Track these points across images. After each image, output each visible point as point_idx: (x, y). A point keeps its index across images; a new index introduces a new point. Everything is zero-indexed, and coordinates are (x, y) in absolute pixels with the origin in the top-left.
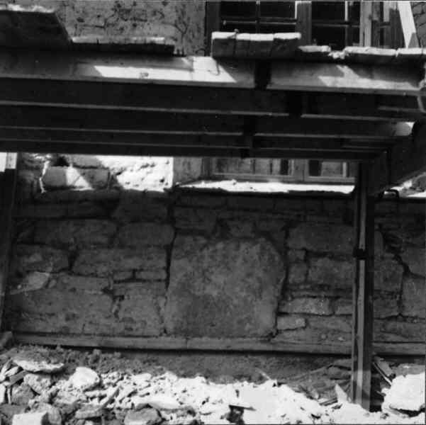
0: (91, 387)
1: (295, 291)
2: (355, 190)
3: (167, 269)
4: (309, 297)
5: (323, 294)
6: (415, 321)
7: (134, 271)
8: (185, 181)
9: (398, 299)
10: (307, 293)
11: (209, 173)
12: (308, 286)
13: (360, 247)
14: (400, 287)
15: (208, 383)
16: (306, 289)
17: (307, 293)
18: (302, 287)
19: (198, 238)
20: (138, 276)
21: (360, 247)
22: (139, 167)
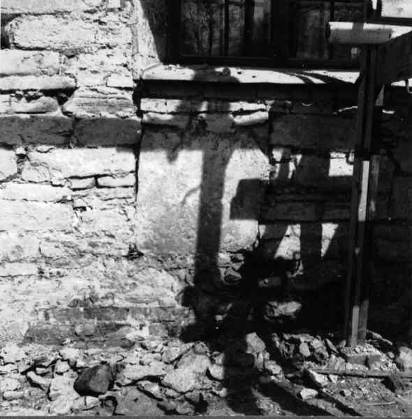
0: (136, 158)
1: (279, 195)
2: (360, 74)
3: (136, 172)
4: (294, 201)
5: (310, 197)
6: (404, 223)
7: (97, 177)
8: (320, 371)
9: (387, 200)
10: (292, 197)
11: (132, 172)
12: (293, 189)
13: (365, 147)
14: (389, 187)
15: (174, 165)
16: (291, 193)
17: (292, 197)
18: (287, 190)
19: (169, 135)
20: (101, 181)
21: (365, 147)
22: (121, 63)
